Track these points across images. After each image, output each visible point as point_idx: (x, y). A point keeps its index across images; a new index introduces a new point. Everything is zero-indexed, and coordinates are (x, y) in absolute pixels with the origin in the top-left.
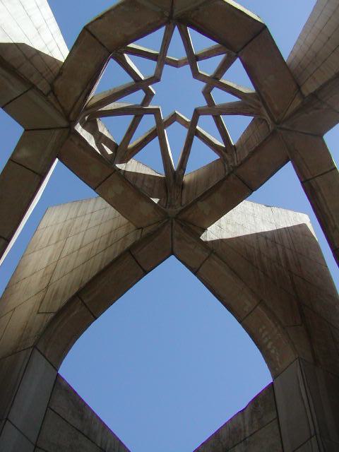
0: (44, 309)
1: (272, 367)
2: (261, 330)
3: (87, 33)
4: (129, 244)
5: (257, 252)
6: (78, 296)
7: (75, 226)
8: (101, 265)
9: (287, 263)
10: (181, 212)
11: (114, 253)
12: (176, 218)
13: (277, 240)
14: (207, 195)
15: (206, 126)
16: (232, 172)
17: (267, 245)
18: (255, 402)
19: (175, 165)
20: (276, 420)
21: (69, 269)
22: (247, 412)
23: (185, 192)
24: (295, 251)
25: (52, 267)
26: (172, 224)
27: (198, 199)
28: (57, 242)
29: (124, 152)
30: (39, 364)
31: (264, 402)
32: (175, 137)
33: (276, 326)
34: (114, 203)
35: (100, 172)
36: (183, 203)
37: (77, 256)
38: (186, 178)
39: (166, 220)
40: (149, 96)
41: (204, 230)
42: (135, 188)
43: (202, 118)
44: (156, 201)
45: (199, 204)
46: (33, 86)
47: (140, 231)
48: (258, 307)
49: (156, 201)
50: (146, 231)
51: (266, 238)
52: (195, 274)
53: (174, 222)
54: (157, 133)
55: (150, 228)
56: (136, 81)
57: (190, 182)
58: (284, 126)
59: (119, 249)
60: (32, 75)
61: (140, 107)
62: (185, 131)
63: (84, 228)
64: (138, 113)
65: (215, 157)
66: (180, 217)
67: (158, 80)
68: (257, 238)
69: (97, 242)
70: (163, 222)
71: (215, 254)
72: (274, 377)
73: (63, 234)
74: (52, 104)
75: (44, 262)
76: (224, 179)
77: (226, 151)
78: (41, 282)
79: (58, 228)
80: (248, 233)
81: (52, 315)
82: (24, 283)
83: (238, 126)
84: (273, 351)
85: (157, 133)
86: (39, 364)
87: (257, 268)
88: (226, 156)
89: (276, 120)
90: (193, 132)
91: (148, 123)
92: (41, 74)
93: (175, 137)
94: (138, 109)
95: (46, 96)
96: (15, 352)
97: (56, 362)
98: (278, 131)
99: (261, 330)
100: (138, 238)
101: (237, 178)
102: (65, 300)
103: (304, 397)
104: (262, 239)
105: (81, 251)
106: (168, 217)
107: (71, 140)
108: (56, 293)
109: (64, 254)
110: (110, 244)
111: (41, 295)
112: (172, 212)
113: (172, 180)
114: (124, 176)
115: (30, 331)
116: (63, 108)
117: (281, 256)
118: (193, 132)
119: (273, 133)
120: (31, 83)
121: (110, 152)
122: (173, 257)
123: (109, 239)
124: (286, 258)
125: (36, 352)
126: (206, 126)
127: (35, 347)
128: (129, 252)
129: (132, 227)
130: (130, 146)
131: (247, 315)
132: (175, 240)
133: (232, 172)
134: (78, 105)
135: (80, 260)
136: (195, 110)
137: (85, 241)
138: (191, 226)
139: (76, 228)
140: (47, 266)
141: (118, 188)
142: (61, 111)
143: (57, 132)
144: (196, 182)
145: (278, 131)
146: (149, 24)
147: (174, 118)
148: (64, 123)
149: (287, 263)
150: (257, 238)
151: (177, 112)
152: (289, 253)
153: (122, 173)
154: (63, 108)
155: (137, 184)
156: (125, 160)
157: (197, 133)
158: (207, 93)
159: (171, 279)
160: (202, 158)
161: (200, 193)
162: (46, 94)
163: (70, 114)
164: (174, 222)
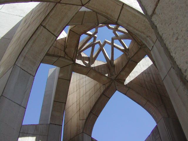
0: (81, 118)
1: (156, 120)
2: (150, 109)
3: (71, 31)
4: (102, 91)
5: (143, 81)
6: (91, 112)
7: (81, 83)
8: (95, 101)
9: (154, 80)
10: (116, 77)
11: (98, 95)
12: (115, 80)
13: (150, 72)
14: (123, 69)
15: (117, 44)
16: (129, 60)
17: (146, 76)
18: (153, 132)
19: (109, 58)
20: (160, 138)
21: (85, 102)
22: (151, 135)
23: (115, 68)
24: (156, 74)
25: (78, 101)
26: (114, 82)
27: (121, 72)
28: (77, 90)
29: (92, 60)
30: (86, 136)
31: (155, 131)
32: (107, 50)
33: (154, 107)
34: (94, 78)
35: (87, 71)
36: (116, 73)
37: (86, 96)
38: (115, 62)
39: (112, 81)
40: (95, 38)
41: (125, 80)
42: (99, 73)
43: (115, 41)
44: (107, 75)
45: (121, 73)
46: (60, 57)
47: (104, 85)
48: (147, 102)
49: (107, 75)
50: (107, 85)
51: (146, 73)
52: (125, 95)
53: (115, 81)
54: (101, 49)
55: (108, 84)
56: (90, 36)
57: (116, 63)
58: (143, 46)
59: (98, 94)
60: (58, 53)
61: (93, 43)
62: (110, 47)
63: (84, 84)
64: (93, 45)
65: (122, 53)
66: (116, 79)
67: (97, 32)
68: (143, 75)
69: (91, 90)
70: (111, 79)
71: (131, 88)
72: (157, 123)
73: (78, 86)
74: (67, 59)
75: (75, 100)
76: (127, 63)
77: (125, 51)
78: (77, 108)
79: (75, 84)
80: (139, 74)
81: (85, 120)
82: (71, 108)
83: (127, 43)
84: (155, 115)
85: (101, 49)
86: (86, 136)
87: (145, 88)
88: (126, 53)
89: (140, 45)
90: (113, 47)
91: (97, 47)
92: (60, 49)
93: (107, 50)
94: (93, 44)
95: (64, 57)
96: (77, 135)
97: (90, 135)
98: (142, 48)
99: (150, 109)
100: (105, 88)
101: (131, 62)
102: (87, 114)
103: (166, 129)
104: (144, 74)
105: (87, 94)
106: (112, 80)
107: (76, 66)
108: (83, 112)
109: (81, 96)
110: (96, 91)
111: (79, 113)
112: (113, 77)
113: (110, 65)
114: (94, 69)
115: (80, 127)
116: (70, 58)
117: (152, 80)
118: (113, 47)
119: (140, 48)
120: (59, 56)
121: (87, 62)
122: (117, 91)
123: (95, 89)
124: (153, 78)
125: (84, 134)
126: (117, 44)
127: (83, 132)
128: (103, 94)
129: (101, 85)
130: (94, 56)
131: (144, 106)
132: (116, 86)
133: (129, 60)
134: (75, 55)
135: (88, 98)
136: (112, 39)
137: (86, 90)
138: (120, 81)
139: (82, 84)
140: (77, 101)
141: (94, 74)
142: (70, 59)
143: (71, 65)
144: (118, 63)
145: (142, 48)
146: (92, 27)
147: (105, 42)
148: (72, 62)
149: (154, 80)
150: (143, 75)
151: (106, 40)
152: (154, 76)
153: (94, 69)
154: (70, 58)
155: (100, 71)
156: (93, 62)
157: (115, 46)
158: (114, 33)
159: (118, 99)
160: (118, 54)
161: (121, 69)
162: (64, 56)
163: (73, 59)
164: (115, 81)
